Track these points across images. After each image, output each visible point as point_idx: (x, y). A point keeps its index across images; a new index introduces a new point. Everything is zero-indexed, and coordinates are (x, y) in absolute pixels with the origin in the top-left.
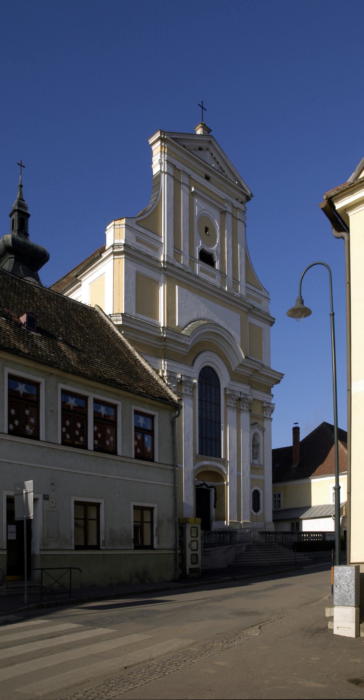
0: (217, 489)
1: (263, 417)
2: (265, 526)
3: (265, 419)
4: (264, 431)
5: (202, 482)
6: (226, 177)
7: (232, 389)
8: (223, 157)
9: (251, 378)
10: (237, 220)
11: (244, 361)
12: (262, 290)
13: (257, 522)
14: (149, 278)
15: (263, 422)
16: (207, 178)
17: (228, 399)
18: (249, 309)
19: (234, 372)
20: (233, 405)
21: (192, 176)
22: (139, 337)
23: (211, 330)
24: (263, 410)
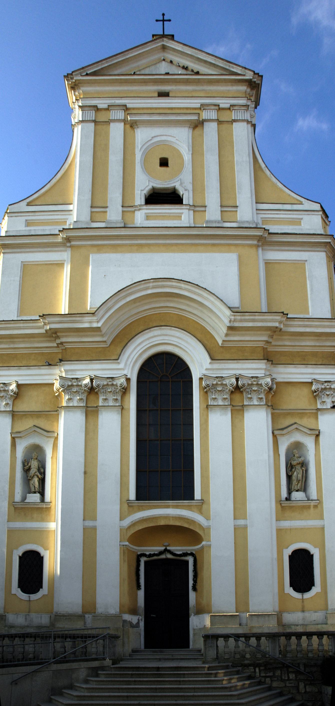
0: (197, 558)
1: (314, 411)
2: (326, 618)
3: (319, 413)
4: (318, 436)
5: (163, 548)
6: (198, 73)
7: (215, 376)
8: (190, 53)
9: (270, 349)
10: (232, 124)
11: (235, 321)
12: (302, 204)
13: (303, 611)
14: (46, 264)
15: (317, 418)
16: (163, 95)
17: (209, 394)
18: (260, 238)
19: (221, 347)
20: (221, 403)
21: (129, 106)
22: (16, 346)
23: (149, 292)
24: (315, 397)
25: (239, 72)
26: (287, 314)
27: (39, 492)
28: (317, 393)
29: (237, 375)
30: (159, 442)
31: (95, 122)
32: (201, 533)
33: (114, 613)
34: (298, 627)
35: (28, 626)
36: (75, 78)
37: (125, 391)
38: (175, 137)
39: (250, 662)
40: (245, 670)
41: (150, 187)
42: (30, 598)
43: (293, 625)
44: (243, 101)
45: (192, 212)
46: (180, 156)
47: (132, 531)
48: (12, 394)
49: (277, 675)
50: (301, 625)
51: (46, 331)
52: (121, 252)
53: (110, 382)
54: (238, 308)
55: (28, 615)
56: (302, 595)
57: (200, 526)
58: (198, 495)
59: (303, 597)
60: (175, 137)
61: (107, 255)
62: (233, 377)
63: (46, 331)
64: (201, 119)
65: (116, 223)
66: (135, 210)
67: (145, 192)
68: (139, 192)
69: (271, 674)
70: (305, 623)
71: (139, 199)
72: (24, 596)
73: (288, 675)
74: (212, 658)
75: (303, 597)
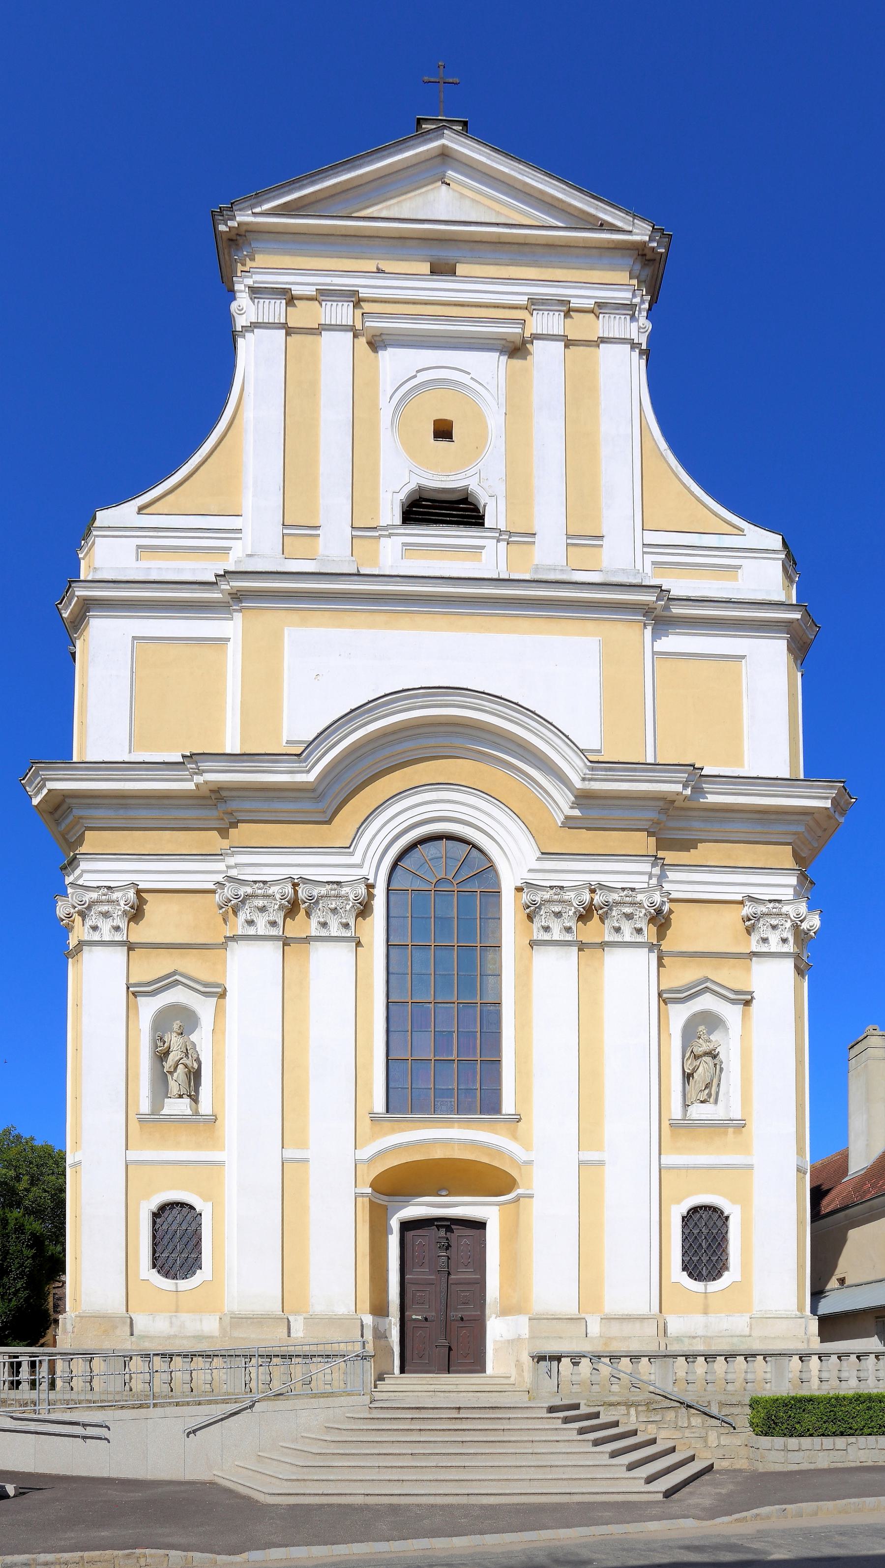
13: (706, 1312)
21: (364, 293)
25: (619, 224)
26: (702, 769)
27: (190, 1096)
28: (753, 921)
29: (593, 883)
30: (432, 1006)
31: (284, 326)
32: (514, 1173)
33: (346, 1313)
34: (694, 1341)
35: (175, 1336)
36: (238, 219)
37: (364, 910)
38: (469, 374)
39: (620, 1399)
40: (609, 1411)
41: (412, 486)
42: (177, 1287)
43: (686, 1337)
44: (624, 296)
45: (503, 545)
46: (480, 418)
47: (379, 1169)
48: (127, 908)
49: (669, 1419)
50: (701, 1337)
51: (197, 785)
52: (352, 627)
53: (331, 890)
54: (599, 751)
55: (175, 1316)
56: (706, 1286)
57: (513, 1160)
58: (508, 1106)
59: (706, 1289)
60: (469, 374)
61: (322, 630)
62: (584, 888)
63: (197, 785)
64: (527, 334)
65: (393, 948)
66: (380, 536)
67: (402, 496)
68: (389, 495)
69: (658, 1418)
70: (709, 1334)
71: (391, 514)
72: (167, 1284)
73: (689, 1419)
74: (549, 1392)
75: (706, 1289)
